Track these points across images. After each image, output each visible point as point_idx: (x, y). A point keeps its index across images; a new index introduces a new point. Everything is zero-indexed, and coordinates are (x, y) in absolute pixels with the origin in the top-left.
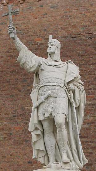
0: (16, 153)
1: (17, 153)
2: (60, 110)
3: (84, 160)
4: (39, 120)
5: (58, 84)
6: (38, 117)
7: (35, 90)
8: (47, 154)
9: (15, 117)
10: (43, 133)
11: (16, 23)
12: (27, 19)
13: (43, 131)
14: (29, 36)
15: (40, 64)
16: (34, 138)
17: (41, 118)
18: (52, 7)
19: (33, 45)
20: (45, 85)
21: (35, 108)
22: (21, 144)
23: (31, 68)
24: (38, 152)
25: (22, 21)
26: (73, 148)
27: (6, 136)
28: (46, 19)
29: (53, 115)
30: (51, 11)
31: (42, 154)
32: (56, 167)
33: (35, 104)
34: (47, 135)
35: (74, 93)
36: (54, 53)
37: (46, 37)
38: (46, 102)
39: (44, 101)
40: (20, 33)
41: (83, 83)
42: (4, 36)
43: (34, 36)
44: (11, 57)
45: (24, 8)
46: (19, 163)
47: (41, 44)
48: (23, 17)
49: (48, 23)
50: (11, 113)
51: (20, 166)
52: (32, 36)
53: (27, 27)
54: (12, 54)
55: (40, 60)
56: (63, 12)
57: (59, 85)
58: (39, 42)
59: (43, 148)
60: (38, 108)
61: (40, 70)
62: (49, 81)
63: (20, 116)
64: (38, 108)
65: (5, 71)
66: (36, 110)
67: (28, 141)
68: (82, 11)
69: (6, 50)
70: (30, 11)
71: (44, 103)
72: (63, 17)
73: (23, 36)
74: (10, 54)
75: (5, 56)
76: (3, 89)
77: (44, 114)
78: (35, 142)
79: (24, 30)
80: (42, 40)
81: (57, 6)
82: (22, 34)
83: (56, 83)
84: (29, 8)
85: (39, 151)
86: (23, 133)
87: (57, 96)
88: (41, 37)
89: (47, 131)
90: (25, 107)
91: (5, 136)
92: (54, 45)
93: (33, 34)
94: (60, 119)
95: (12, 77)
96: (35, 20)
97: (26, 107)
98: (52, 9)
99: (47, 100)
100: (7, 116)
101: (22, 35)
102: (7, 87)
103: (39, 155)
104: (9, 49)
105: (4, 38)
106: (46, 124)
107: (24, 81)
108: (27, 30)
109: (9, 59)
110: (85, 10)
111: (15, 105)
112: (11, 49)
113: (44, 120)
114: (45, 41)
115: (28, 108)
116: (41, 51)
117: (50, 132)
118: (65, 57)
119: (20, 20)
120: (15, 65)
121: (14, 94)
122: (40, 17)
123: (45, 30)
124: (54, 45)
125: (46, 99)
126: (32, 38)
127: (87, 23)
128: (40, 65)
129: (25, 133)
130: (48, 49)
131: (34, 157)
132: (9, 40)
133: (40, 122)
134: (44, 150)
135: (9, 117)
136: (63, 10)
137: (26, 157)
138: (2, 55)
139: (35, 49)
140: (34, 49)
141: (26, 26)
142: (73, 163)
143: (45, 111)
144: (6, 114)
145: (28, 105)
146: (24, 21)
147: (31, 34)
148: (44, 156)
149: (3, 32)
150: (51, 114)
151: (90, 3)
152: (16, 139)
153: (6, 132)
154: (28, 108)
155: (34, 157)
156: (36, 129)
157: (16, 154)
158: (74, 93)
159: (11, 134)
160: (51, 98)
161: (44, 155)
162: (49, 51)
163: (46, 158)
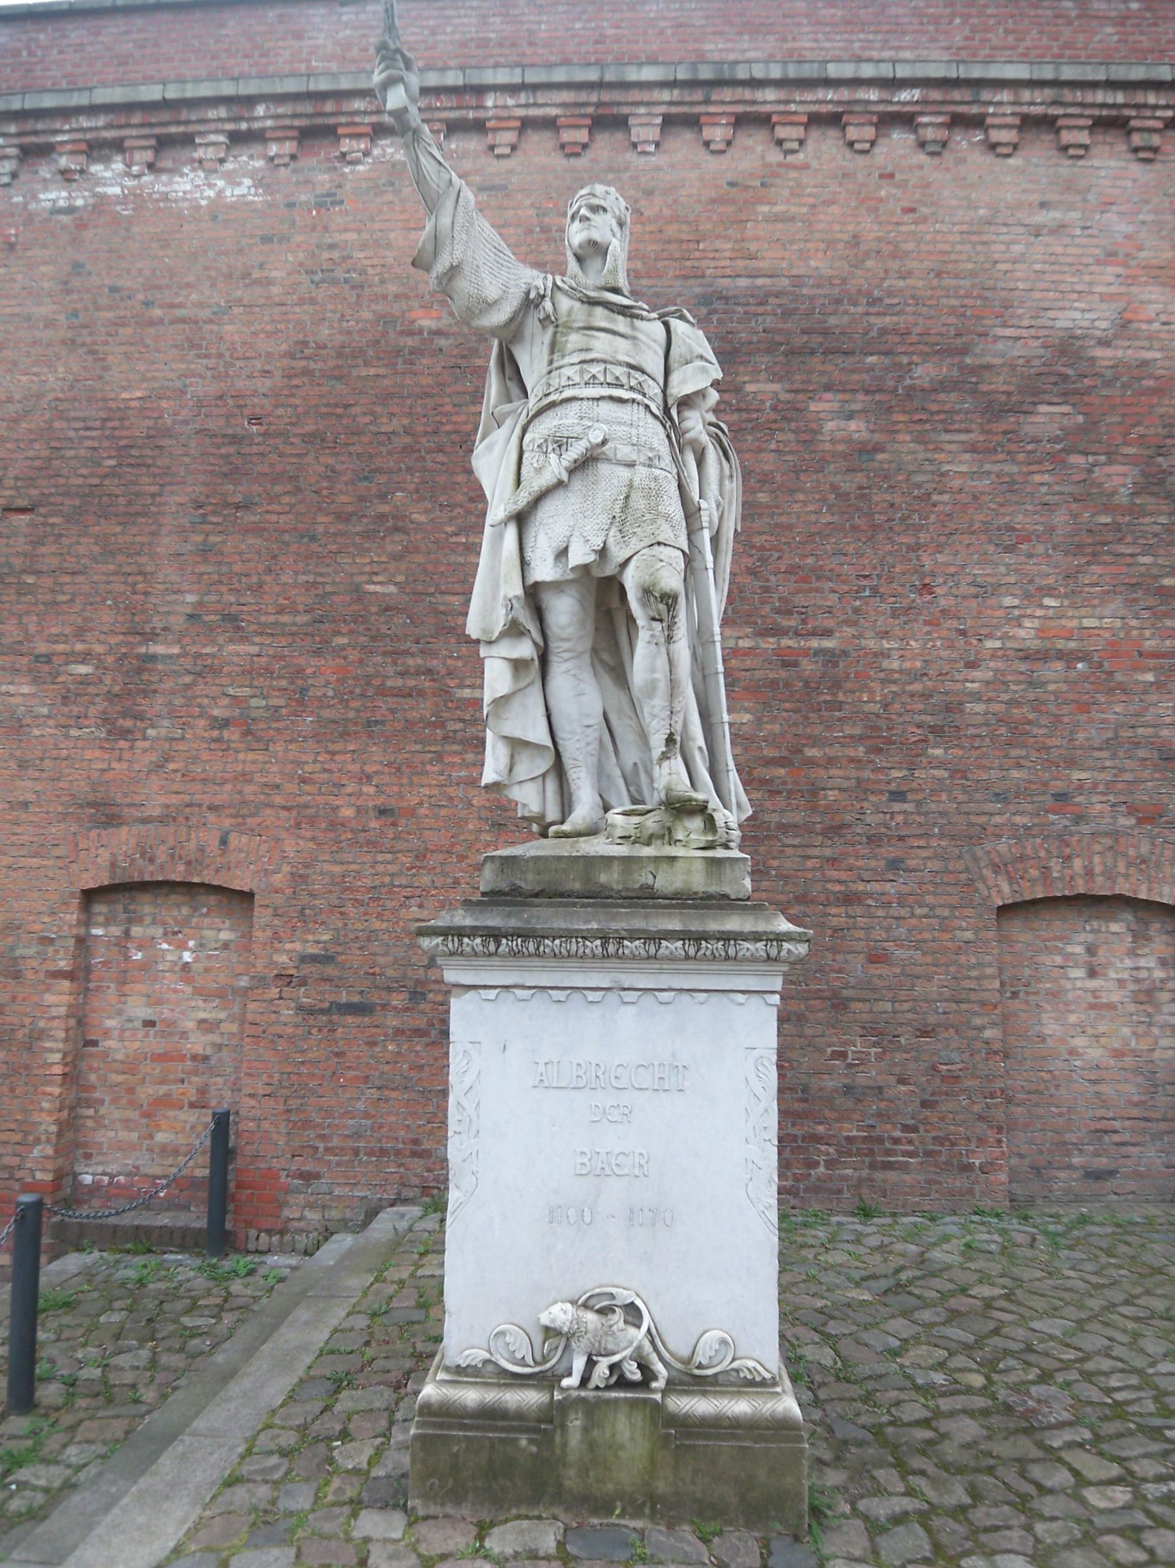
0: (325, 770)
1: (330, 771)
3: (739, 805)
4: (530, 581)
5: (639, 397)
6: (524, 563)
7: (499, 435)
8: (559, 768)
9: (322, 626)
11: (330, 241)
12: (377, 226)
13: (541, 643)
14: (385, 297)
15: (532, 295)
16: (497, 678)
17: (544, 570)
19: (402, 333)
20: (568, 393)
21: (505, 522)
22: (344, 735)
23: (490, 306)
24: (512, 757)
25: (354, 236)
26: (694, 740)
27: (282, 702)
29: (618, 554)
31: (534, 766)
32: (632, 832)
33: (500, 503)
35: (700, 462)
38: (577, 484)
39: (565, 477)
40: (346, 281)
42: (275, 290)
43: (407, 297)
44: (306, 379)
45: (364, 184)
47: (438, 333)
50: (301, 608)
51: (343, 825)
52: (397, 296)
53: (375, 261)
54: (312, 365)
56: (533, 212)
57: (647, 401)
58: (426, 323)
59: (540, 735)
60: (521, 520)
62: (594, 377)
64: (521, 520)
65: (276, 435)
66: (511, 533)
69: (284, 347)
70: (389, 197)
71: (560, 494)
72: (531, 231)
73: (359, 296)
74: (302, 363)
75: (278, 373)
76: (270, 508)
77: (562, 554)
78: (502, 702)
80: (439, 319)
81: (505, 187)
82: (353, 287)
83: (631, 388)
85: (517, 745)
86: (358, 691)
87: (634, 457)
89: (567, 645)
91: (274, 702)
93: (401, 290)
95: (310, 459)
97: (371, 588)
99: (578, 476)
100: (285, 619)
101: (354, 292)
102: (286, 499)
103: (516, 769)
104: (297, 343)
105: (277, 300)
106: (564, 612)
107: (360, 480)
108: (378, 270)
109: (297, 386)
111: (321, 575)
112: (305, 344)
113: (557, 586)
115: (378, 588)
117: (583, 653)
119: (346, 230)
120: (325, 410)
121: (321, 529)
126: (396, 309)
131: (489, 776)
132: (297, 309)
133: (534, 594)
134: (549, 744)
135: (294, 624)
136: (532, 205)
137: (369, 789)
138: (267, 367)
139: (411, 353)
140: (406, 351)
143: (571, 532)
144: (281, 611)
146: (365, 235)
147: (392, 288)
148: (544, 776)
149: (274, 274)
150: (603, 553)
152: (326, 713)
153: (284, 683)
155: (489, 776)
156: (514, 630)
157: (325, 776)
158: (700, 462)
159: (303, 691)
160: (604, 468)
163: (551, 786)
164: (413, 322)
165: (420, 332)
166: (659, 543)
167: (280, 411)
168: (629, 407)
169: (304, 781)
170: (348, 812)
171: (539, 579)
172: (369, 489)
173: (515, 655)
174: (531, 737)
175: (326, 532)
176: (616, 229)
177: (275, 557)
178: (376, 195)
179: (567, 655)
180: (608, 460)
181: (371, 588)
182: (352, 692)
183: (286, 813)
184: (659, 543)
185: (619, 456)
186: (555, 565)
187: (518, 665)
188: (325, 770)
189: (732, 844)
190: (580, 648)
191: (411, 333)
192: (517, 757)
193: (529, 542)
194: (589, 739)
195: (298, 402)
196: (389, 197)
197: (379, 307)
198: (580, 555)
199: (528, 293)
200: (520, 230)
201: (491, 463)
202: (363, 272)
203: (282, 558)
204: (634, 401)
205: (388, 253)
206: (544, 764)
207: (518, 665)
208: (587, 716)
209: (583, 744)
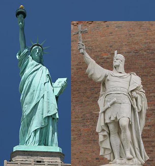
0: (85, 150)
1: (86, 151)
2: (124, 115)
4: (105, 122)
5: (122, 92)
7: (102, 97)
8: (112, 152)
10: (109, 134)
11: (85, 41)
12: (95, 37)
13: (109, 132)
14: (97, 51)
15: (106, 75)
16: (101, 138)
17: (108, 121)
18: (117, 27)
19: (100, 59)
21: (102, 113)
22: (89, 143)
23: (99, 79)
24: (105, 150)
28: (111, 37)
30: (116, 30)
33: (102, 109)
34: (113, 135)
36: (119, 66)
37: (111, 52)
38: (112, 107)
39: (110, 106)
41: (144, 91)
43: (101, 51)
44: (81, 70)
45: (92, 28)
46: (88, 160)
47: (108, 58)
48: (91, 35)
49: (114, 40)
50: (80, 117)
51: (89, 162)
52: (99, 51)
53: (95, 44)
55: (107, 72)
57: (124, 93)
58: (105, 56)
59: (109, 147)
60: (104, 112)
61: (106, 81)
63: (89, 119)
64: (104, 112)
65: (75, 81)
66: (103, 114)
67: (95, 140)
68: (144, 30)
69: (76, 64)
70: (97, 30)
73: (91, 52)
76: (73, 97)
77: (110, 118)
78: (102, 142)
79: (92, 47)
80: (108, 55)
81: (121, 26)
82: (90, 50)
83: (121, 91)
84: (96, 28)
85: (105, 149)
88: (107, 53)
90: (93, 112)
91: (75, 137)
92: (119, 59)
93: (100, 50)
94: (124, 122)
95: (81, 86)
96: (102, 38)
97: (94, 112)
98: (117, 29)
100: (77, 119)
101: (90, 51)
105: (74, 54)
106: (111, 127)
108: (95, 46)
109: (79, 71)
110: (146, 29)
112: (80, 62)
113: (109, 123)
114: (111, 55)
115: (96, 112)
116: (108, 64)
117: (116, 133)
118: (128, 69)
120: (84, 76)
121: (84, 100)
122: (106, 35)
123: (111, 46)
124: (119, 59)
125: (111, 105)
126: (99, 53)
127: (148, 41)
128: (106, 76)
129: (93, 134)
130: (114, 62)
131: (101, 154)
134: (110, 148)
137: (94, 154)
139: (102, 63)
140: (101, 62)
141: (94, 43)
142: (135, 160)
144: (76, 118)
145: (96, 110)
147: (98, 50)
148: (110, 153)
150: (116, 118)
151: (151, 24)
152: (85, 139)
154: (96, 112)
155: (101, 154)
156: (103, 130)
157: (85, 152)
158: (136, 100)
160: (116, 104)
161: (110, 152)
162: (115, 64)
164: (102, 56)
165: (104, 58)
166: (124, 117)
167: (75, 76)
168: (120, 94)
169: (81, 153)
170: (89, 159)
171: (107, 122)
172: (94, 92)
173: (104, 134)
174: (107, 147)
175: (85, 101)
176: (121, 62)
177: (75, 107)
178: (95, 30)
179: (112, 134)
180: (117, 103)
181: (94, 112)
182: (90, 134)
183: (77, 160)
184: (124, 117)
185: (119, 102)
186: (109, 120)
187: (104, 136)
188: (85, 150)
189: (136, 164)
190: (115, 132)
191: (102, 59)
192: (105, 151)
193: (105, 116)
194: (117, 147)
195: (79, 75)
196: (97, 30)
197: (96, 54)
198: (113, 119)
199: (105, 75)
200: (124, 35)
201: (101, 102)
202: (92, 47)
203: (76, 107)
204: (121, 93)
205: (97, 42)
206: (110, 152)
207: (104, 136)
208: (117, 143)
209: (116, 148)
